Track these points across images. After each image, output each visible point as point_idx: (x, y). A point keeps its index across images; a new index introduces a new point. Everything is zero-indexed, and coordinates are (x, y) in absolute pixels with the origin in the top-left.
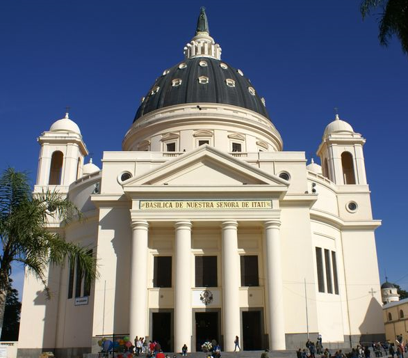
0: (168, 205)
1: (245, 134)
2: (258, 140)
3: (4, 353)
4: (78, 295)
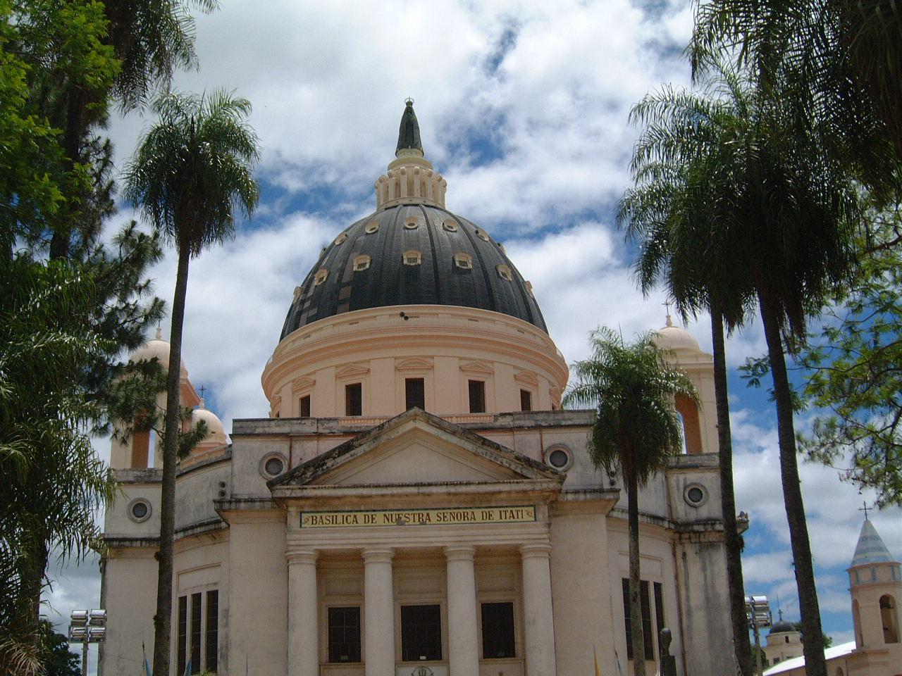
0: (351, 519)
2: (517, 372)
4: (197, 598)
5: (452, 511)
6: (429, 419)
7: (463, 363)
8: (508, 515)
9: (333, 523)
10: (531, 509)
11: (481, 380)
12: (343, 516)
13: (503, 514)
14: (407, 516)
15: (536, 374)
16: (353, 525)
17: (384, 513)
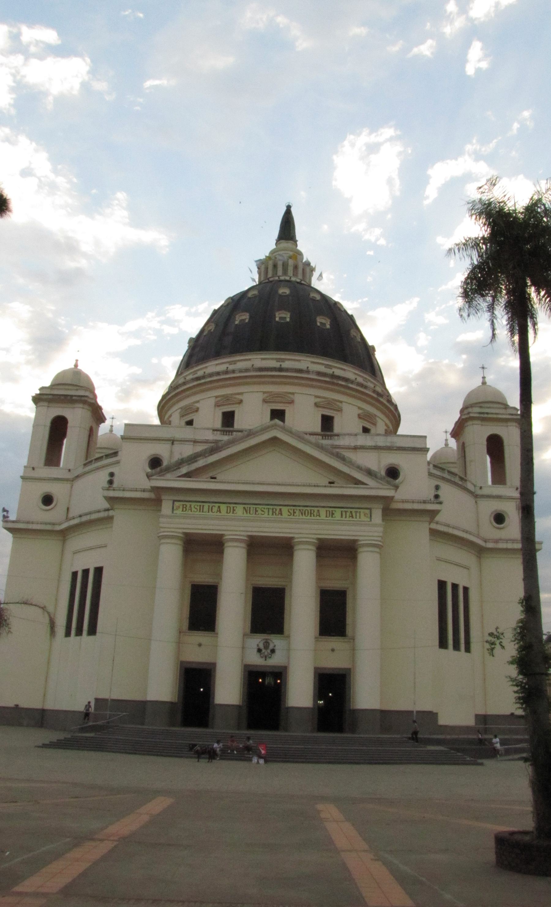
0: (215, 509)
1: (341, 402)
3: (356, 305)
4: (79, 632)
5: (301, 508)
6: (290, 432)
7: (318, 400)
8: (348, 514)
9: (200, 511)
10: (367, 511)
11: (332, 415)
12: (209, 506)
13: (344, 514)
14: (263, 509)
15: (376, 415)
16: (217, 514)
17: (244, 506)
